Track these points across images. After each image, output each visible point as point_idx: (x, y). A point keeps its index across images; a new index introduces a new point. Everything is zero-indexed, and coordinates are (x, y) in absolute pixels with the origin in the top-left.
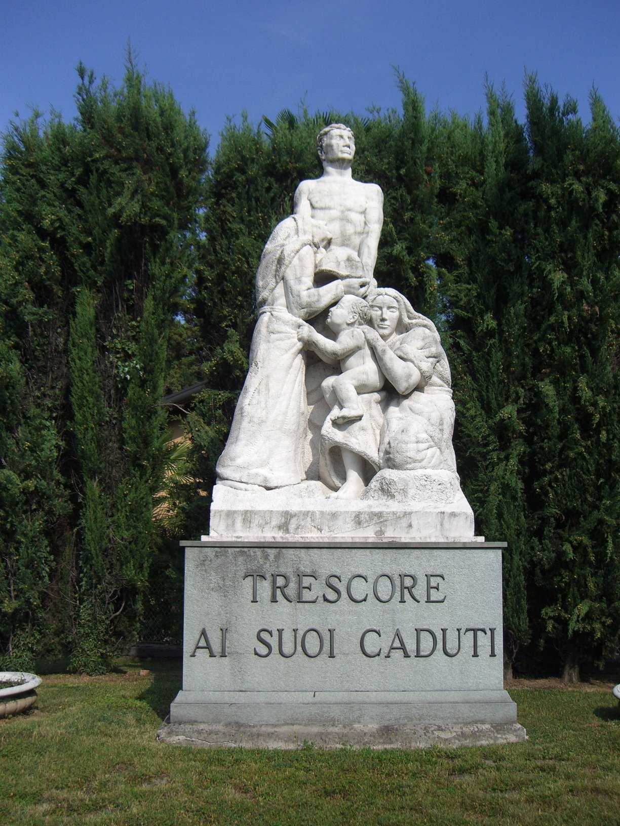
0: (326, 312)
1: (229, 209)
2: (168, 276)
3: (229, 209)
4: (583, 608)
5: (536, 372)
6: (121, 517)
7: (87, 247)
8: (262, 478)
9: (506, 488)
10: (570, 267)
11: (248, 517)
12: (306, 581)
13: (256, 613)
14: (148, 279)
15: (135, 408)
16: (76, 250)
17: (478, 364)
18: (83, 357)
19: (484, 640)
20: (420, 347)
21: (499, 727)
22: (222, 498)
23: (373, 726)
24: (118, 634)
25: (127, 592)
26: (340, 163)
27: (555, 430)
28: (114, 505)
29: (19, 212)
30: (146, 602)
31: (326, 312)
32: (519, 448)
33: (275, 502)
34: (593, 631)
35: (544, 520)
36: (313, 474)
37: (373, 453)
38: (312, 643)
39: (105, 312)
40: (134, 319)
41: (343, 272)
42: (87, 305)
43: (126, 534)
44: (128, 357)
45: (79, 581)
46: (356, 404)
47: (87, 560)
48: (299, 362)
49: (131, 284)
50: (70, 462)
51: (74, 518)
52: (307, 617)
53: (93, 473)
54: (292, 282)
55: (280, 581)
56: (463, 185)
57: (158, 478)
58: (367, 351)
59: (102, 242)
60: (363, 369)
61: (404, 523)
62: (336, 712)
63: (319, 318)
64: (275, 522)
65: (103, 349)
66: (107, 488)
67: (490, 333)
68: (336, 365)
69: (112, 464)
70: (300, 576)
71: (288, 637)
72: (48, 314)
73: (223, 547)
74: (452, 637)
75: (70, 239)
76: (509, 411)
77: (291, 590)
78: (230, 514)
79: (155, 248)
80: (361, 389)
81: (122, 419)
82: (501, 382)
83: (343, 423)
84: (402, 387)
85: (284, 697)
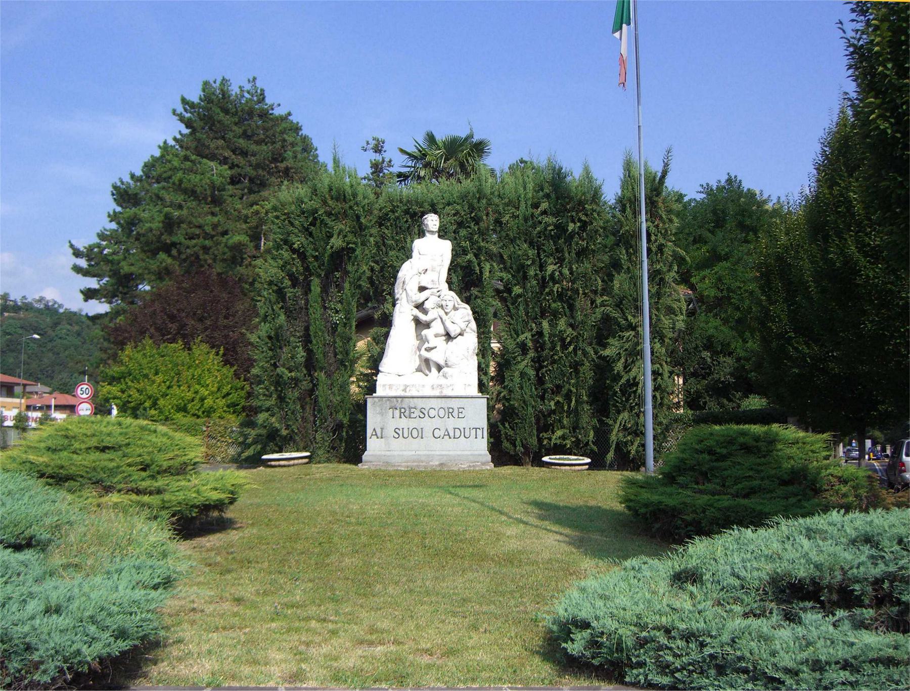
0: (423, 303)
1: (386, 231)
2: (356, 271)
3: (386, 231)
4: (559, 433)
5: (543, 315)
6: (336, 390)
7: (316, 258)
8: (399, 369)
9: (523, 375)
10: (561, 261)
11: (391, 386)
12: (412, 410)
13: (394, 422)
14: (347, 273)
15: (342, 337)
16: (311, 259)
17: (513, 311)
18: (316, 312)
19: (479, 432)
20: (462, 316)
21: (483, 464)
22: (381, 379)
23: (437, 463)
24: (333, 448)
25: (339, 426)
26: (432, 232)
27: (549, 345)
28: (332, 384)
29: (282, 240)
30: (347, 432)
31: (423, 303)
32: (532, 354)
33: (402, 381)
34: (566, 445)
35: (545, 391)
36: (419, 370)
37: (442, 363)
38: (415, 433)
39: (325, 289)
40: (339, 292)
41: (429, 286)
42: (316, 286)
43: (338, 398)
44: (337, 312)
45: (315, 421)
46: (433, 342)
47: (320, 411)
48: (413, 324)
49: (338, 274)
50: (310, 364)
51: (311, 392)
52: (412, 423)
53: (321, 369)
54: (409, 292)
55: (403, 410)
56: (507, 217)
57: (353, 371)
58: (439, 320)
59: (323, 255)
60: (437, 328)
61: (451, 388)
62: (423, 459)
63: (420, 306)
64: (402, 388)
65: (325, 308)
66: (329, 375)
67: (519, 296)
68: (427, 325)
69: (330, 365)
70: (410, 408)
71: (406, 431)
72: (299, 291)
73: (382, 397)
74: (467, 431)
75: (308, 254)
76: (526, 336)
77: (407, 414)
78: (384, 386)
79: (350, 258)
80: (436, 336)
81: (335, 342)
82: (524, 321)
83: (429, 350)
84: (452, 335)
85: (405, 453)
